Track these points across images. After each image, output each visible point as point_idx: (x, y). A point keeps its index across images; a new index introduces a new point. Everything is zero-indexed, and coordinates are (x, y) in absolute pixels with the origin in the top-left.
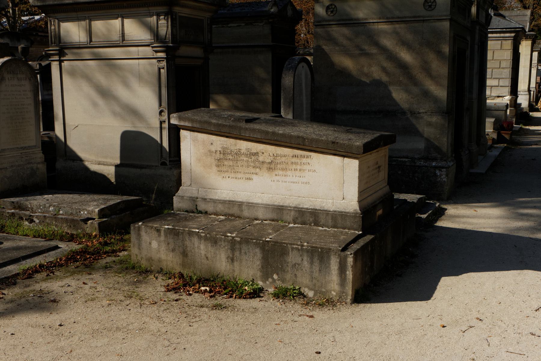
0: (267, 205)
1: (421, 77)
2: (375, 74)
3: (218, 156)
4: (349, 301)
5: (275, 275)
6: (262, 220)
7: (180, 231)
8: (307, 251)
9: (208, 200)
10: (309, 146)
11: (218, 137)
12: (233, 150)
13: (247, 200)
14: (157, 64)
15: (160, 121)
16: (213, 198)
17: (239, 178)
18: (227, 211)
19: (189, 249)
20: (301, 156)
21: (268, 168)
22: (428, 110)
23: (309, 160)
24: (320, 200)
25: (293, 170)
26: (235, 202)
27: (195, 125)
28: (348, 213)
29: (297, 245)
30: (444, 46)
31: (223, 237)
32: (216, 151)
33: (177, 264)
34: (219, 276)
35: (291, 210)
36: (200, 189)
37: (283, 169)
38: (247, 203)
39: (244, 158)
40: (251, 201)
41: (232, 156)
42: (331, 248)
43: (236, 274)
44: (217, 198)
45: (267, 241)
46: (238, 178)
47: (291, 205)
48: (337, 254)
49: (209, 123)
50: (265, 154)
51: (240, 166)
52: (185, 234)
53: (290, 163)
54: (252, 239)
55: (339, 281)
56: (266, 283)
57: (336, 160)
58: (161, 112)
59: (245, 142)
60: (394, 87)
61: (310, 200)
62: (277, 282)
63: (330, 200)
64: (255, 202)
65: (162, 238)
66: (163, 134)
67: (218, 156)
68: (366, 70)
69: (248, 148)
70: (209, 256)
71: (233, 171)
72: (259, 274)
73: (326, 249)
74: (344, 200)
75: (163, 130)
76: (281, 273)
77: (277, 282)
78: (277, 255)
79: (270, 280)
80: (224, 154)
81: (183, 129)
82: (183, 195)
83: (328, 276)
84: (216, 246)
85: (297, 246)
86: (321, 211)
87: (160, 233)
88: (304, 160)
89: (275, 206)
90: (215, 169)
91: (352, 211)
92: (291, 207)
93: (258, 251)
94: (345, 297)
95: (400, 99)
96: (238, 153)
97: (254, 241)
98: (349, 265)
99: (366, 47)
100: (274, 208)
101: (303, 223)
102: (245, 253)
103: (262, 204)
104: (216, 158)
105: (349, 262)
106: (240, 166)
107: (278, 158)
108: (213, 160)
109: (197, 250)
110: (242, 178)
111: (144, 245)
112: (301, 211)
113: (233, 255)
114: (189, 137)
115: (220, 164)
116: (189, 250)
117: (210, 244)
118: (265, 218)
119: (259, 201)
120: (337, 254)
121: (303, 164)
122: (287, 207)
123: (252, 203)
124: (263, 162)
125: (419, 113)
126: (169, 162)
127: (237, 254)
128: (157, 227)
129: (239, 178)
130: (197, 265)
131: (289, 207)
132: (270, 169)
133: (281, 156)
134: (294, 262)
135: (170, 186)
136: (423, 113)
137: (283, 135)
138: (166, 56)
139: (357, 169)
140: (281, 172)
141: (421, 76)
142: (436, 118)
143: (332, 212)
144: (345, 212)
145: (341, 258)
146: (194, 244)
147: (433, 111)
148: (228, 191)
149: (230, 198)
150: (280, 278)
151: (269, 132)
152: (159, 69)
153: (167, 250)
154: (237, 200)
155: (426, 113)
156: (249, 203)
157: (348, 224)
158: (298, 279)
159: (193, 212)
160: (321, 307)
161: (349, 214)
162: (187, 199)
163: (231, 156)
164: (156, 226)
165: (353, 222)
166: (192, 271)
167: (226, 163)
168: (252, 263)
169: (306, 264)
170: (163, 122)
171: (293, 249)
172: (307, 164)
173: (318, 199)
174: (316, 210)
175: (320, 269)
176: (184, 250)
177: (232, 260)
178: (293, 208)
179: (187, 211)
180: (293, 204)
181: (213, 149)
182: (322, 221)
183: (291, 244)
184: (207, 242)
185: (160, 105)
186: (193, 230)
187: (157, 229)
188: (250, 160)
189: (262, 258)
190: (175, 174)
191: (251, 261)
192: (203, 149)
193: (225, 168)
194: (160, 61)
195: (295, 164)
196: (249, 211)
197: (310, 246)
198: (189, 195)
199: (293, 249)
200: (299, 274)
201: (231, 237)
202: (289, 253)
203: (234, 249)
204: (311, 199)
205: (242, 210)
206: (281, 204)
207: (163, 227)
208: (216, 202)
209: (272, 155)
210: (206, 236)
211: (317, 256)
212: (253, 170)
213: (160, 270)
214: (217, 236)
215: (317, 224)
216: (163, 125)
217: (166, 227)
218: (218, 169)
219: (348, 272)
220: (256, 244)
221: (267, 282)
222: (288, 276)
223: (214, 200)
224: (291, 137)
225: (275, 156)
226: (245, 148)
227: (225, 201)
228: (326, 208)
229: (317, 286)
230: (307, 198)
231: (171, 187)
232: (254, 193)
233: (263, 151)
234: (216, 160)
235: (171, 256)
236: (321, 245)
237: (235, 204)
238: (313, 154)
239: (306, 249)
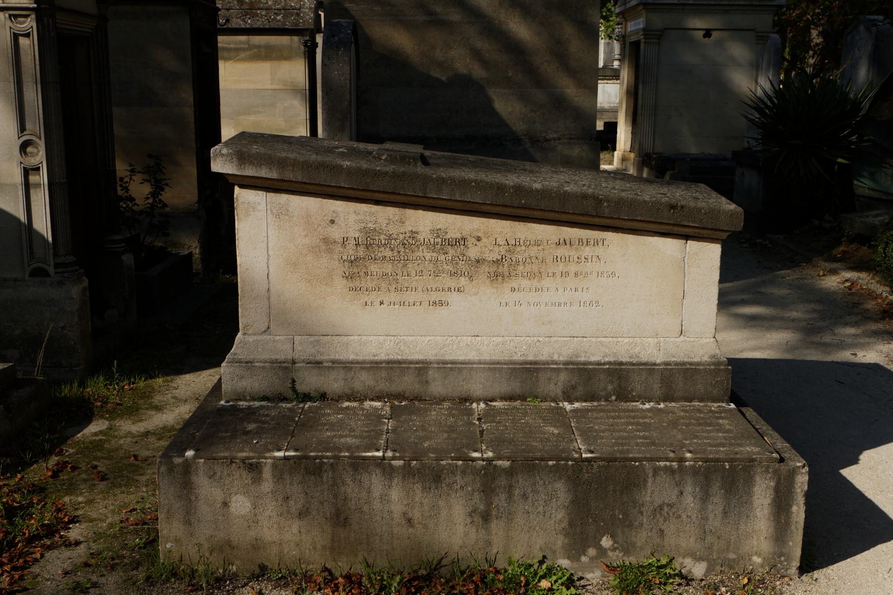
0: (493, 363)
1: (548, 70)
2: (458, 64)
3: (351, 252)
4: (793, 570)
5: (604, 538)
6: (488, 400)
7: (325, 461)
8: (695, 471)
9: (325, 364)
10: (612, 218)
11: (350, 204)
12: (395, 236)
13: (436, 355)
14: (9, 23)
15: (24, 168)
16: (341, 358)
17: (411, 304)
18: (383, 386)
19: (352, 505)
20: (580, 241)
21: (492, 274)
22: (563, 135)
23: (599, 250)
24: (626, 340)
25: (558, 274)
26: (405, 363)
27: (289, 175)
28: (698, 365)
29: (667, 459)
30: (591, 12)
31: (460, 462)
32: (345, 240)
33: (315, 548)
34: (444, 562)
35: (558, 370)
36: (297, 338)
37: (531, 276)
38: (438, 363)
39: (425, 255)
40: (448, 358)
41: (392, 250)
42: (754, 457)
43: (495, 551)
44: (352, 357)
45: (587, 459)
46: (406, 303)
47: (556, 357)
48: (771, 470)
49: (336, 169)
50: (484, 240)
51: (413, 273)
52: (341, 468)
53: (549, 259)
54: (542, 459)
55: (771, 530)
56: (578, 560)
57: (669, 246)
58: (24, 147)
59: (430, 213)
60: (497, 90)
61: (601, 343)
62: (610, 554)
63: (650, 339)
64: (462, 358)
65: (267, 485)
66: (32, 199)
67: (351, 251)
68: (439, 54)
69: (438, 227)
70: (416, 515)
71: (394, 286)
72: (560, 541)
73: (741, 460)
74: (682, 336)
75: (32, 191)
76: (623, 532)
77: (610, 554)
78: (614, 491)
79: (592, 552)
80: (367, 246)
81: (242, 186)
82: (250, 357)
83: (746, 523)
84: (436, 488)
85: (668, 463)
86: (634, 364)
87: (261, 472)
88: (587, 251)
89: (514, 363)
90: (340, 284)
91: (706, 359)
92: (556, 364)
93: (560, 487)
94: (786, 563)
95: (510, 114)
96: (411, 241)
97: (550, 463)
98: (799, 490)
99: (439, 9)
100: (515, 369)
101: (590, 397)
102: (525, 497)
103: (480, 363)
104: (345, 258)
105: (799, 484)
106: (413, 273)
107: (518, 249)
108: (337, 263)
109: (377, 505)
110: (418, 304)
111: (204, 511)
112: (585, 370)
113: (489, 504)
114: (262, 207)
115: (356, 270)
116: (353, 507)
117: (418, 487)
118: (490, 393)
119: (472, 356)
120: (771, 470)
121: (583, 259)
122: (547, 363)
123: (453, 362)
124: (478, 261)
125: (547, 140)
126: (55, 268)
127: (500, 500)
128: (248, 458)
129: (411, 304)
130: (377, 541)
131: (552, 364)
132: (497, 277)
133: (528, 244)
134: (658, 502)
135: (62, 324)
136: (554, 139)
137: (544, 193)
138: (35, 5)
139: (717, 263)
140: (525, 283)
141: (549, 69)
142: (579, 149)
143: (659, 365)
144: (691, 364)
145: (780, 478)
146: (369, 491)
147: (573, 136)
148: (381, 338)
149: (388, 355)
150: (617, 543)
151: (506, 186)
152: (16, 37)
153: (281, 514)
154: (409, 358)
155: (559, 139)
156: (445, 362)
157: (700, 388)
158: (666, 539)
159: (285, 399)
160: (102, 485)
161: (702, 367)
162: (264, 368)
163: (388, 249)
164: (244, 454)
165: (711, 383)
166: (360, 558)
167: (374, 268)
168: (541, 517)
169: (690, 501)
170: (33, 169)
171: (656, 471)
172: (594, 259)
173: (620, 339)
174: (621, 363)
175: (727, 508)
176: (338, 510)
177: (486, 518)
178: (564, 364)
179: (264, 398)
180: (560, 355)
181: (336, 233)
182: (638, 387)
183: (651, 460)
184: (411, 480)
185: (22, 128)
186: (364, 454)
187: (251, 464)
188: (442, 257)
189: (572, 502)
190: (74, 296)
191: (539, 512)
192: (306, 236)
193: (372, 280)
194: (16, 16)
195: (563, 260)
196: (447, 382)
197: (701, 459)
198: (266, 356)
199: (656, 471)
200: (670, 528)
201: (483, 460)
202: (645, 481)
203: (493, 490)
204: (603, 339)
205: (427, 382)
206: (531, 358)
207: (268, 455)
208: (351, 368)
209: (503, 242)
210: (407, 465)
211: (719, 479)
212: (451, 283)
213: (257, 571)
214: (443, 463)
215: (624, 395)
216: (33, 179)
217: (280, 454)
218: (351, 285)
219: (794, 508)
220: (557, 471)
221: (584, 559)
222: (641, 537)
223: (343, 363)
224: (565, 197)
225: (512, 246)
226: (428, 229)
227: (376, 363)
228: (644, 358)
229: (715, 548)
230: (594, 339)
231: (63, 328)
232: (454, 338)
233: (479, 235)
234: (346, 263)
235: (295, 529)
236: (718, 452)
237: (408, 368)
238: (609, 236)
239: (693, 467)
